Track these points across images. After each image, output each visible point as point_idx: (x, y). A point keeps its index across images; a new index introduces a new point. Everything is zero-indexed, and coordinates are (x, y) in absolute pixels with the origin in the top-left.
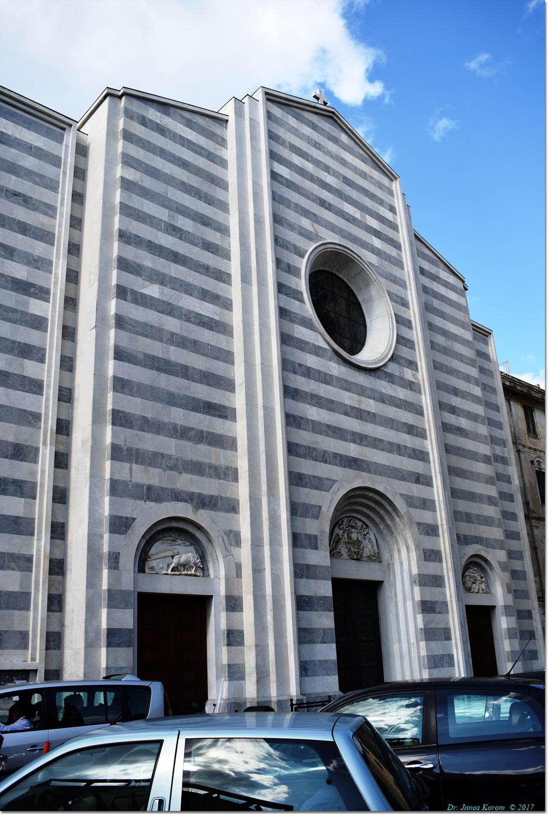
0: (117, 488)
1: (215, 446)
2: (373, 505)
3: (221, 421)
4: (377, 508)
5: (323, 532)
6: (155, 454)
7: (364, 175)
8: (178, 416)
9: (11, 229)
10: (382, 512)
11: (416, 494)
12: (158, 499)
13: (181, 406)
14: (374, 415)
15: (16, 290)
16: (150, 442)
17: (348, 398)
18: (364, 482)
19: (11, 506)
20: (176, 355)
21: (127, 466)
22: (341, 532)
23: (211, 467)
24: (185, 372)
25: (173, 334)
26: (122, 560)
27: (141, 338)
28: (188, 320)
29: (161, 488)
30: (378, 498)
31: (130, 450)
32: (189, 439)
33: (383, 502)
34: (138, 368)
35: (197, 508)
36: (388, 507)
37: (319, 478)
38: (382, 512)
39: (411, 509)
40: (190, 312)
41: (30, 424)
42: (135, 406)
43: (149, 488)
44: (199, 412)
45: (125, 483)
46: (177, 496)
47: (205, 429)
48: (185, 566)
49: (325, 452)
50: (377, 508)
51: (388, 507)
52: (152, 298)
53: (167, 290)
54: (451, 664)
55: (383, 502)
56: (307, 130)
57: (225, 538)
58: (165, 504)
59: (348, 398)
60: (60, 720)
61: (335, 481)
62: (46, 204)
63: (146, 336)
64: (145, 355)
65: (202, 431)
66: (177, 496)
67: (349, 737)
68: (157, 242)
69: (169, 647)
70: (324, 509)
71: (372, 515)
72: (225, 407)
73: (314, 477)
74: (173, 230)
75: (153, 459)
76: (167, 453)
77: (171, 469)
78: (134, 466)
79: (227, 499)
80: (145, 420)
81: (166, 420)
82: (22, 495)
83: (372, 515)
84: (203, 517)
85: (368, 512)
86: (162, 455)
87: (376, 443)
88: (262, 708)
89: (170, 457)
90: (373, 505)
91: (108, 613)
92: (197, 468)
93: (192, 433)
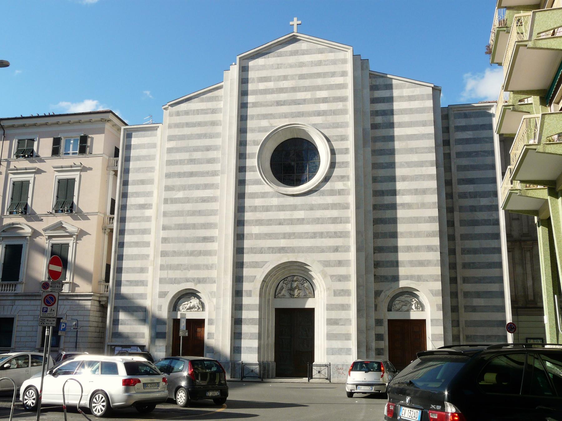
0: (162, 281)
1: (207, 256)
3: (210, 244)
6: (178, 265)
7: (319, 63)
8: (190, 247)
9: (138, 184)
11: (332, 259)
12: (179, 283)
13: (191, 242)
14: (303, 219)
15: (140, 209)
16: (175, 260)
17: (282, 215)
20: (190, 220)
21: (166, 272)
23: (204, 265)
24: (194, 226)
25: (188, 211)
26: (163, 308)
27: (174, 218)
28: (197, 202)
29: (180, 278)
31: (167, 265)
32: (194, 256)
34: (173, 231)
35: (196, 284)
37: (256, 262)
39: (326, 269)
40: (197, 198)
41: (146, 259)
42: (170, 247)
43: (175, 279)
44: (200, 242)
45: (165, 279)
46: (187, 280)
47: (202, 249)
48: (194, 307)
49: (262, 248)
52: (179, 198)
53: (186, 192)
56: (292, 60)
57: (210, 295)
59: (282, 215)
60: (480, 383)
61: (266, 262)
62: (150, 168)
63: (176, 216)
64: (175, 225)
65: (201, 251)
66: (187, 280)
67: (406, 390)
68: (182, 171)
69: (292, 339)
70: (258, 277)
72: (213, 237)
74: (192, 161)
75: (177, 267)
76: (183, 263)
77: (185, 269)
78: (169, 271)
79: (212, 278)
80: (174, 252)
81: (183, 250)
82: (143, 285)
84: (198, 287)
86: (181, 265)
87: (300, 236)
89: (185, 265)
91: (505, 316)
92: (197, 267)
93: (196, 252)
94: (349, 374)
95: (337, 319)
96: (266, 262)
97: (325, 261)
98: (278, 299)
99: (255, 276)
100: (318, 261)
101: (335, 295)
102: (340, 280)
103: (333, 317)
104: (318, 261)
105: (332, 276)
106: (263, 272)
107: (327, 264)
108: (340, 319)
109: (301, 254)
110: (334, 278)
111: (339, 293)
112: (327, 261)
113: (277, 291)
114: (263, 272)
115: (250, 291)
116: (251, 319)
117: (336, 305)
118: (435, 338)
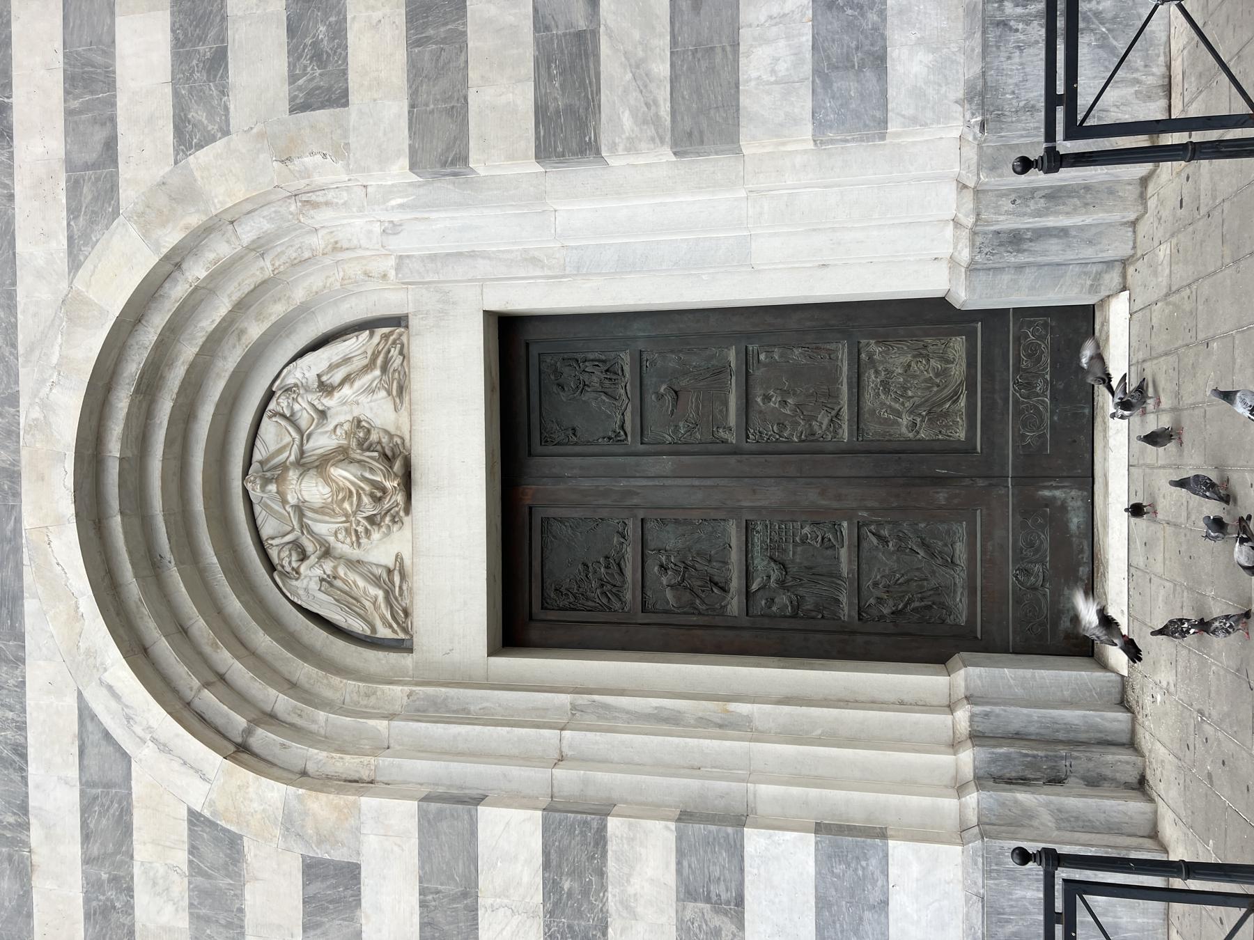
2: (165, 408)
4: (176, 376)
5: (290, 824)
10: (188, 351)
18: (59, 521)
19: (272, 894)
22: (311, 573)
30: (122, 402)
33: (133, 367)
36: (149, 335)
38: (188, 351)
39: (128, 195)
50: (176, 376)
51: (149, 335)
54: (1067, 138)
55: (133, 367)
58: (352, 85)
61: (85, 714)
71: (215, 390)
73: (86, 837)
83: (215, 390)
85: (206, 414)
88: (811, 449)
90: (165, 408)
94: (1023, 856)
95: (545, 60)
96: (85, 714)
97: (73, 212)
98: (422, 620)
99: (195, 818)
100: (75, 264)
101: (337, 97)
102: (218, 62)
103: (523, 98)
104: (75, 264)
105: (187, 137)
106: (164, 748)
107: (93, 181)
108: (541, 23)
109: (28, 412)
110: (198, 114)
111: (318, 57)
112: (74, 188)
113: (357, 626)
114: (164, 748)
115: (313, 869)
116: (551, 887)
117: (415, 73)
118: (957, 347)
